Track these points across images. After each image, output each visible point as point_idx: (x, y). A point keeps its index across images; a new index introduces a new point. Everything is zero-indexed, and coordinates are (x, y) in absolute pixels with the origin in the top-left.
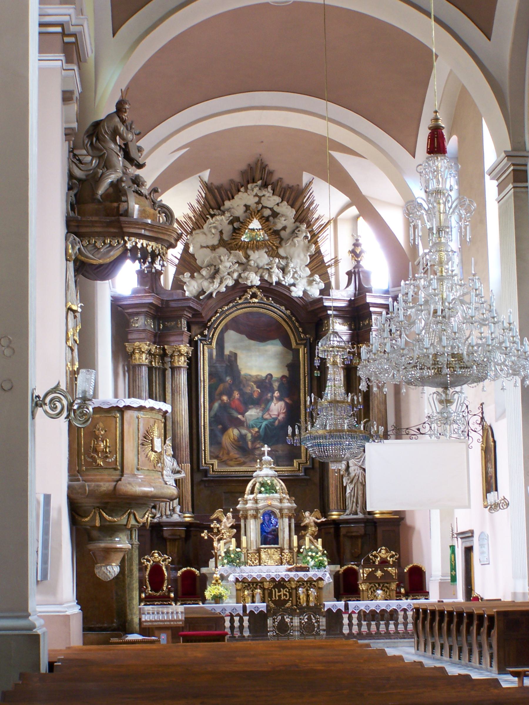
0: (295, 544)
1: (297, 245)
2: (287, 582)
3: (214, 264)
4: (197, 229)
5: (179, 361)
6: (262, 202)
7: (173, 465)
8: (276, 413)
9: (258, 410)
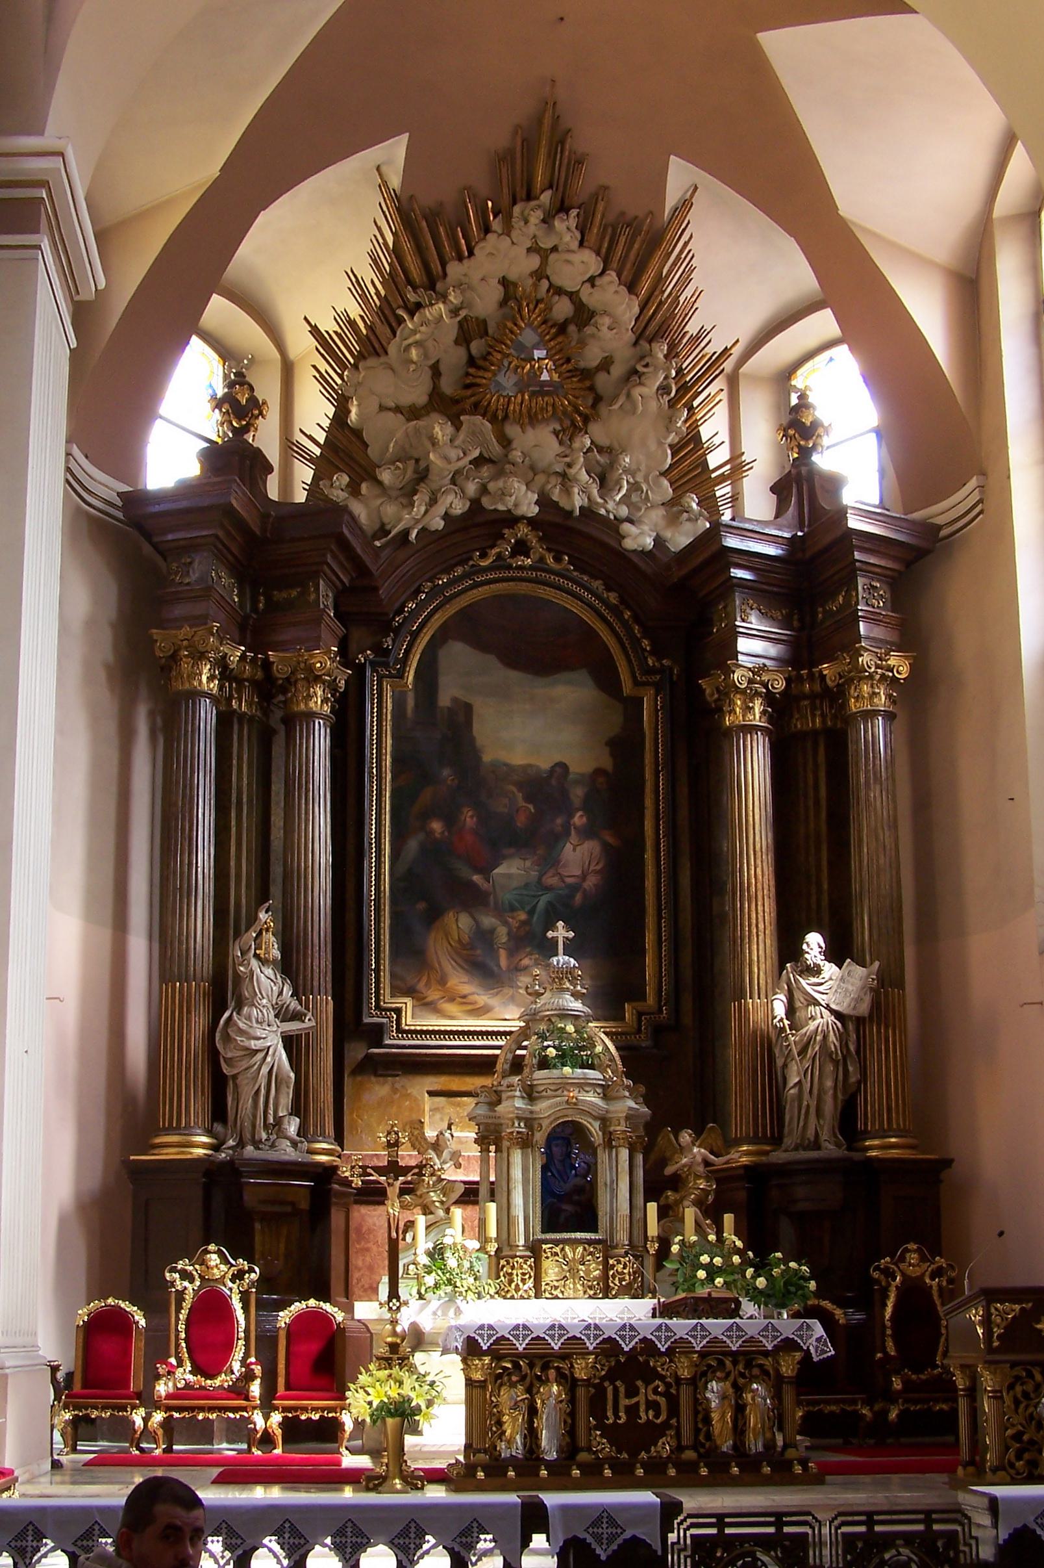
0: (653, 1229)
2: (661, 1354)
3: (416, 456)
4: (370, 355)
5: (309, 697)
7: (281, 993)
8: (578, 872)
9: (528, 863)
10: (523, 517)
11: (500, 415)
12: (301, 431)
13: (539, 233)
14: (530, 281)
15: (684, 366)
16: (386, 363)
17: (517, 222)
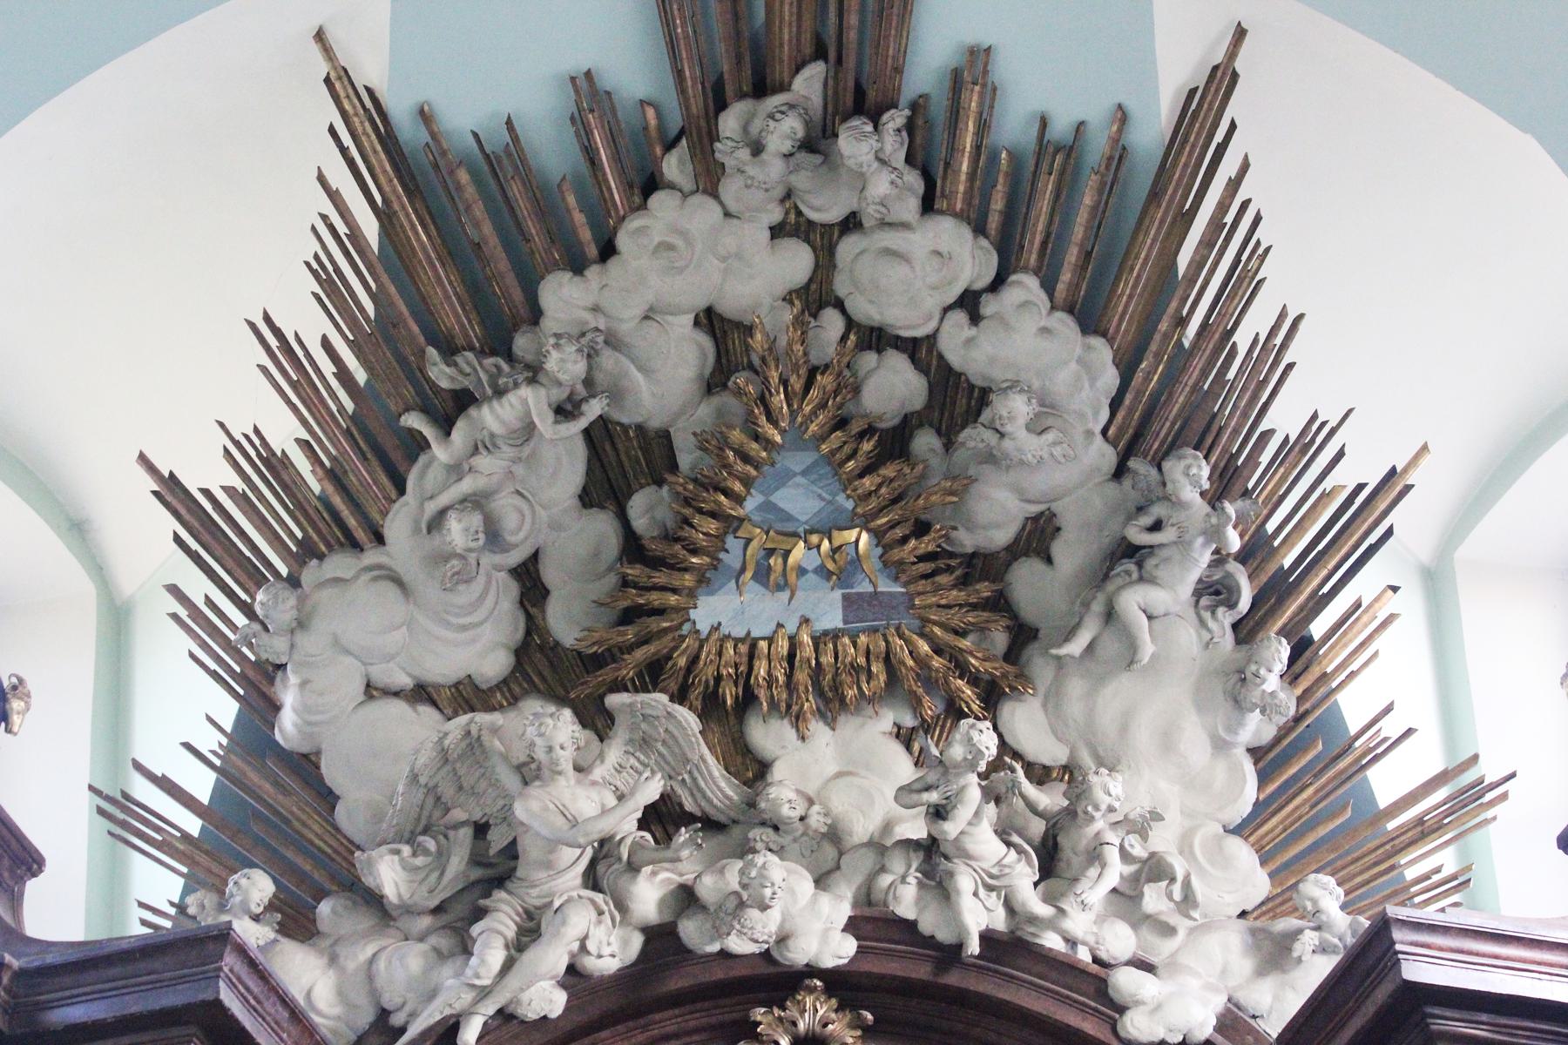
1: (1147, 649)
6: (841, 287)
10: (811, 971)
11: (729, 693)
12: (138, 767)
13: (801, 181)
14: (787, 315)
15: (1271, 527)
16: (379, 567)
17: (729, 151)
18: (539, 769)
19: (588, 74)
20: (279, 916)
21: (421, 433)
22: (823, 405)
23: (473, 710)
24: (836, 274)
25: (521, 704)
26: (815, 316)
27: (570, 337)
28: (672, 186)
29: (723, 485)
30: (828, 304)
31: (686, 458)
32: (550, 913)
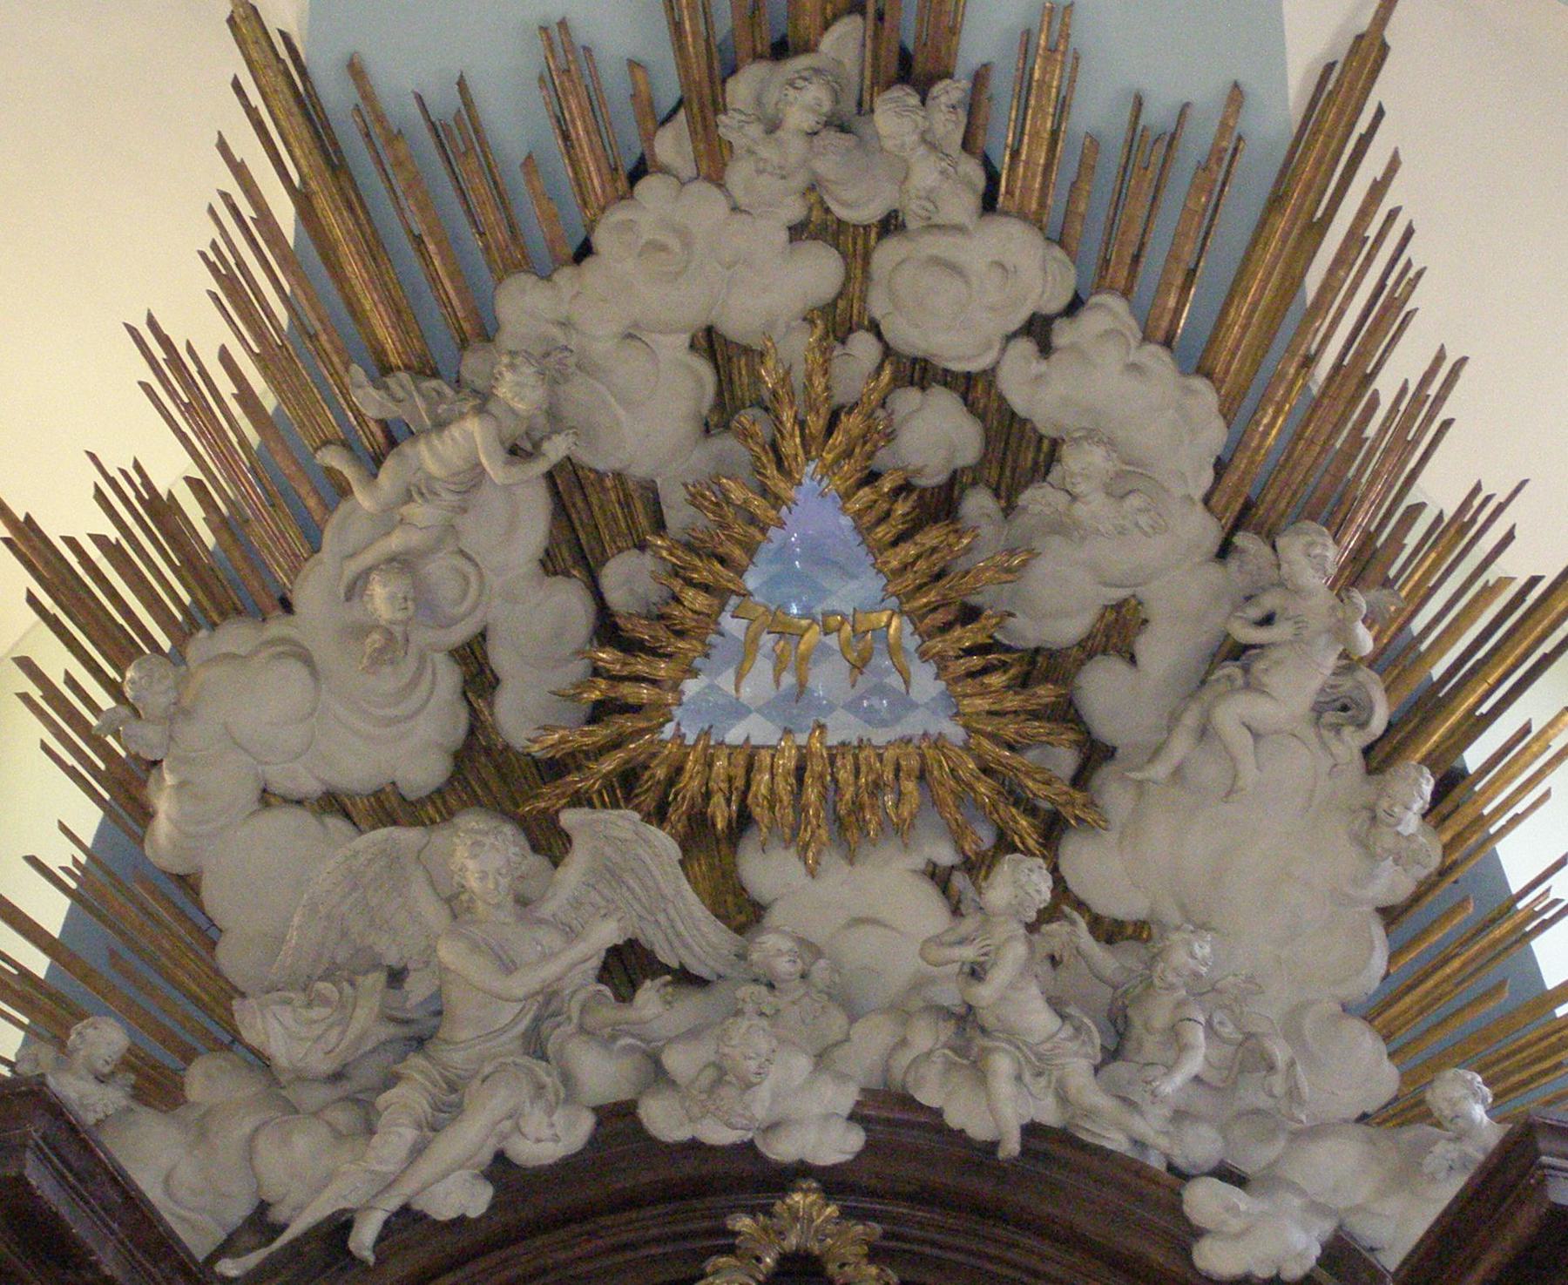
1: (1249, 774)
3: (392, 958)
6: (878, 306)
11: (721, 814)
13: (826, 166)
15: (1417, 625)
16: (283, 640)
18: (471, 900)
19: (563, 24)
20: (133, 1077)
21: (341, 473)
22: (848, 454)
23: (395, 823)
24: (870, 288)
25: (456, 820)
26: (843, 342)
27: (528, 355)
28: (664, 170)
29: (720, 550)
30: (860, 326)
31: (678, 515)
32: (476, 1083)
